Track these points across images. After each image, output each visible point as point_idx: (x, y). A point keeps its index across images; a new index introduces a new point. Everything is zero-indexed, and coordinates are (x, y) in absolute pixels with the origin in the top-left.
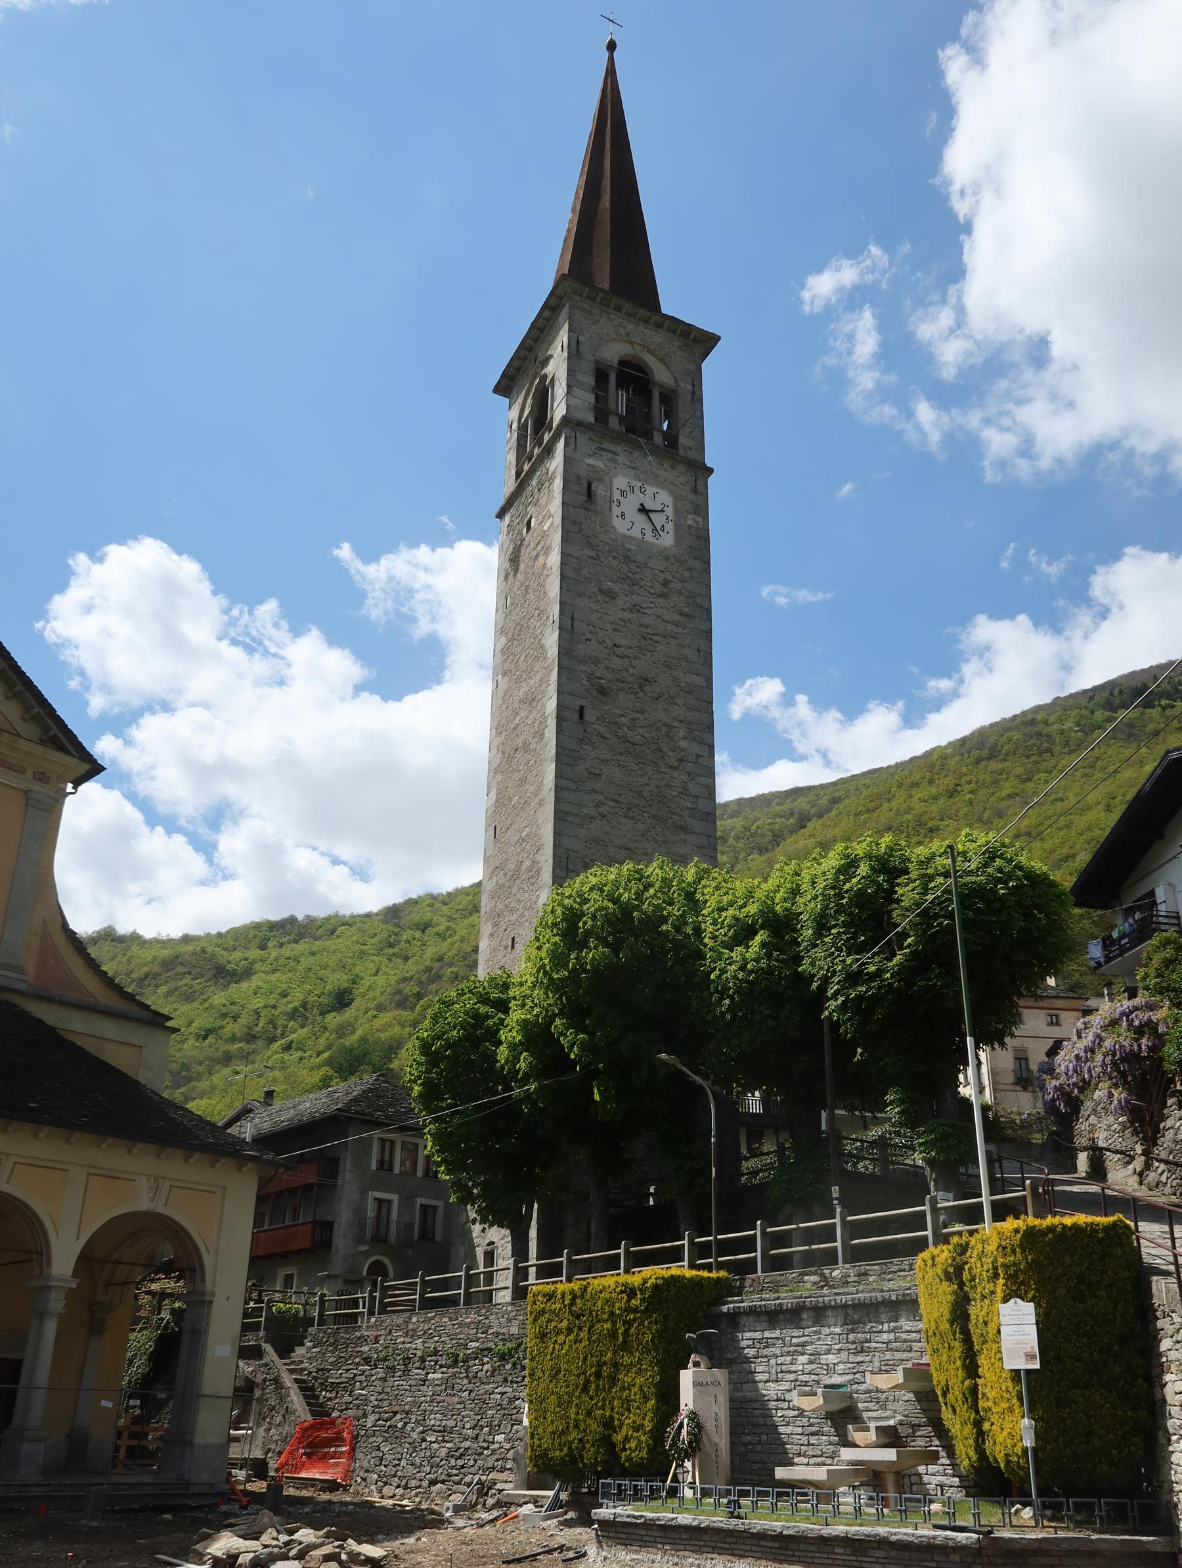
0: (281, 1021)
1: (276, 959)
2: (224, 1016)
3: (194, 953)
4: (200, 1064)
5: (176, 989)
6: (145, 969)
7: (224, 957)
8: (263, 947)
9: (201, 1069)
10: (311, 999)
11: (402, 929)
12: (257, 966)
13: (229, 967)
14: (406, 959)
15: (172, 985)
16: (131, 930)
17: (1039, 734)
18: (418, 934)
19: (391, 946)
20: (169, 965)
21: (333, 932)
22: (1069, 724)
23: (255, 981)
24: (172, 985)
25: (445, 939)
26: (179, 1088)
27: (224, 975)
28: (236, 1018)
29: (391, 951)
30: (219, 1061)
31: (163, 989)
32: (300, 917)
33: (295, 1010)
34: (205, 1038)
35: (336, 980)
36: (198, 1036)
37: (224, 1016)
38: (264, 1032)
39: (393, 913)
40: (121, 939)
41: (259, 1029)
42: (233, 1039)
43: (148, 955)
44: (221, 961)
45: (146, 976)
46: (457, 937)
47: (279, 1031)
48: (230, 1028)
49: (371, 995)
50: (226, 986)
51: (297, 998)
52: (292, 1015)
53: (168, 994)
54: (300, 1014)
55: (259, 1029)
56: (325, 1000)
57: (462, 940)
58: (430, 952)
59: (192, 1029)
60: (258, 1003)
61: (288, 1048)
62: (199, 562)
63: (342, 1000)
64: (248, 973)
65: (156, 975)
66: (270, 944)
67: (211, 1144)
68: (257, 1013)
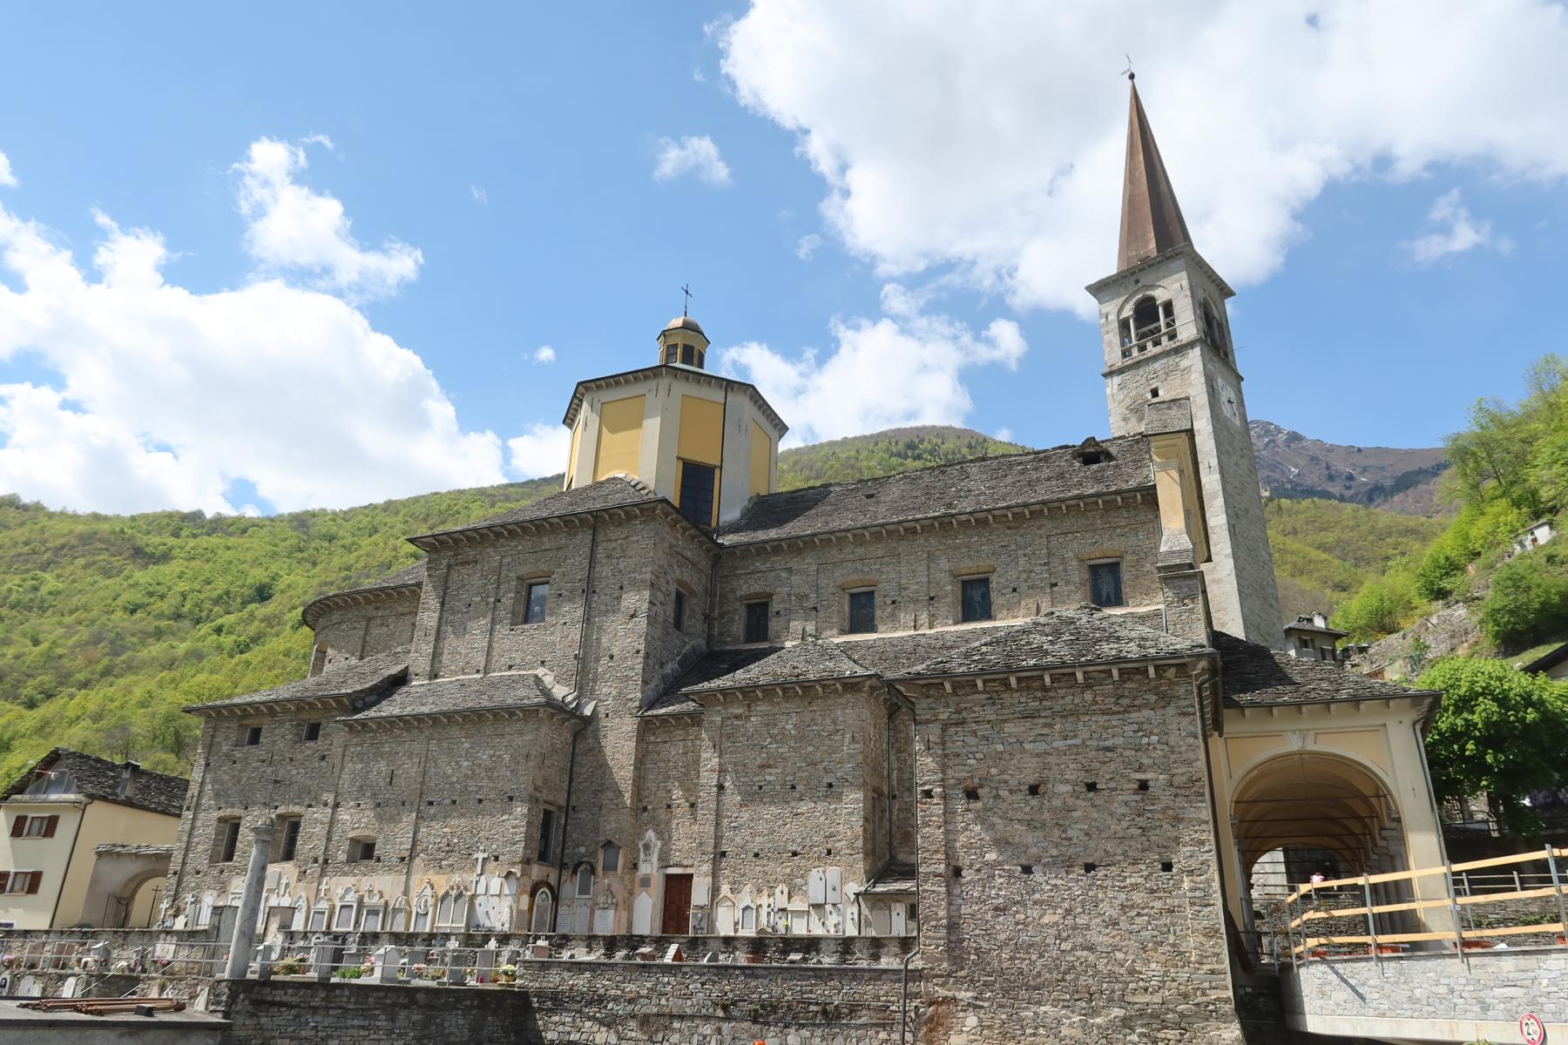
0: (207, 605)
1: (194, 548)
2: (151, 594)
3: (113, 532)
4: (133, 635)
5: (94, 563)
6: (62, 540)
7: (142, 540)
8: (176, 535)
9: (135, 640)
10: (233, 589)
11: (310, 538)
12: (175, 552)
13: (147, 550)
14: (315, 564)
15: (90, 558)
16: (35, 500)
17: (852, 467)
18: (326, 544)
19: (301, 551)
20: (86, 539)
21: (244, 531)
22: (873, 463)
23: (174, 567)
24: (90, 558)
25: (350, 552)
26: (119, 655)
27: (141, 555)
28: (162, 597)
29: (300, 555)
30: (150, 635)
31: (81, 561)
32: (209, 515)
33: (220, 597)
34: (133, 612)
35: (258, 575)
36: (125, 609)
37: (151, 594)
38: (190, 612)
39: (301, 521)
40: (26, 508)
41: (186, 609)
42: (160, 616)
43: (65, 527)
44: (139, 543)
45: (63, 547)
46: (362, 552)
47: (204, 614)
48: (159, 606)
49: (292, 593)
50: (145, 566)
51: (220, 586)
52: (217, 601)
53: (85, 567)
54: (223, 600)
55: (186, 609)
56: (246, 592)
57: (368, 555)
58: (336, 562)
59: (119, 602)
60: (183, 586)
61: (219, 630)
62: (154, 229)
63: (263, 594)
64: (165, 557)
65: (72, 547)
66: (184, 533)
67: (1319, 633)
68: (184, 596)
